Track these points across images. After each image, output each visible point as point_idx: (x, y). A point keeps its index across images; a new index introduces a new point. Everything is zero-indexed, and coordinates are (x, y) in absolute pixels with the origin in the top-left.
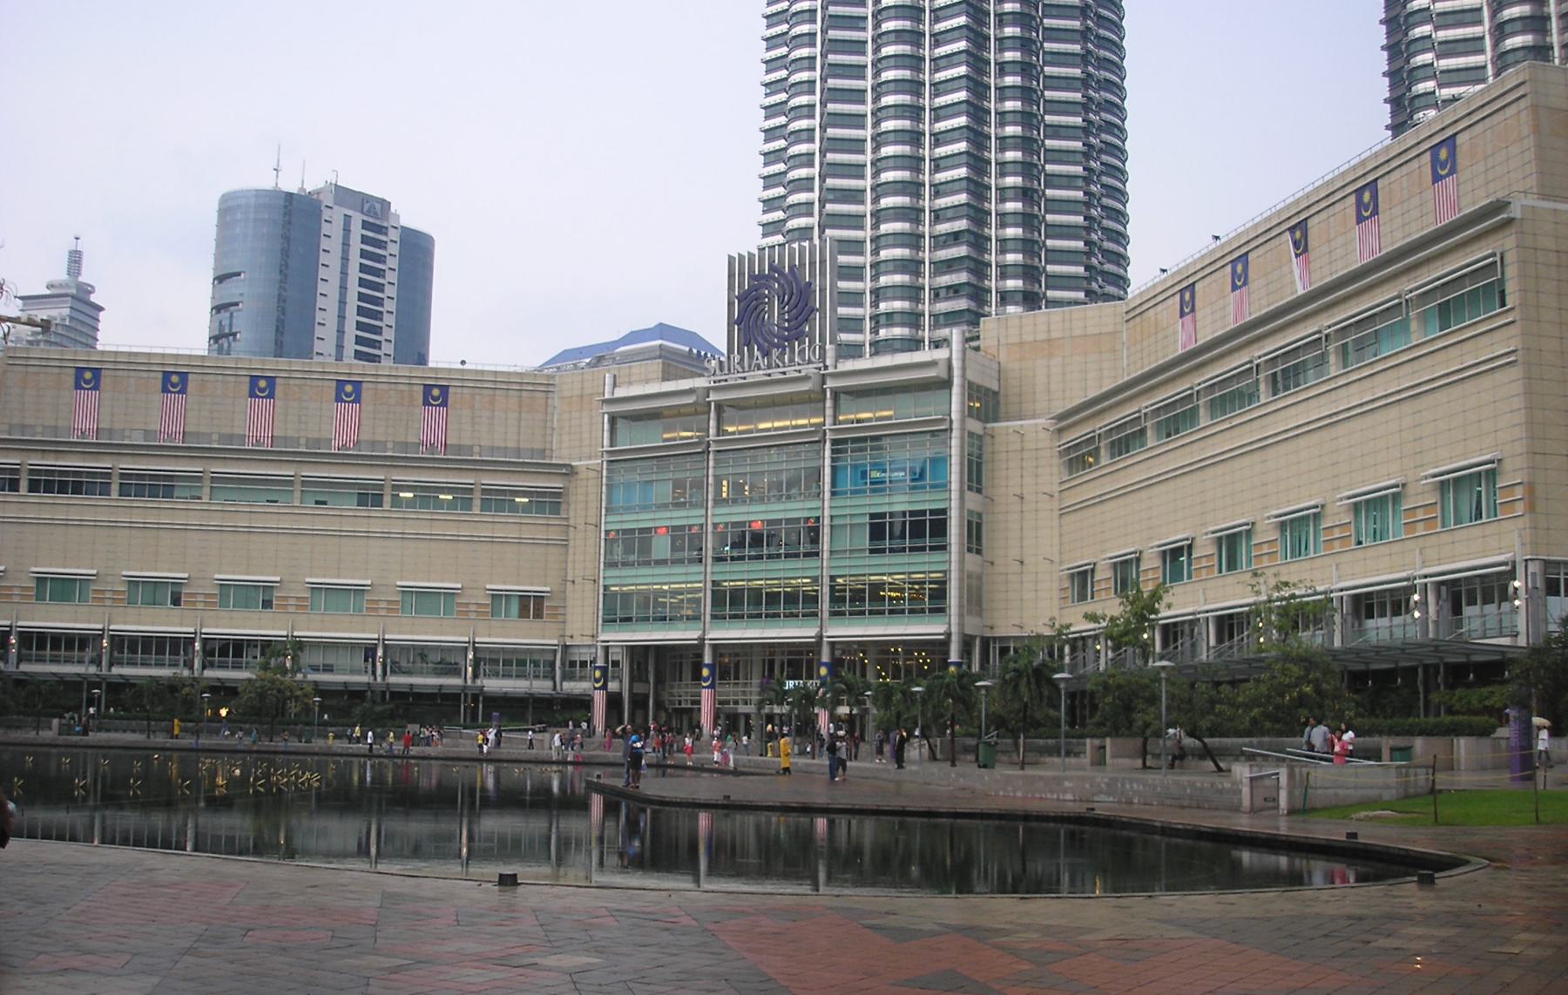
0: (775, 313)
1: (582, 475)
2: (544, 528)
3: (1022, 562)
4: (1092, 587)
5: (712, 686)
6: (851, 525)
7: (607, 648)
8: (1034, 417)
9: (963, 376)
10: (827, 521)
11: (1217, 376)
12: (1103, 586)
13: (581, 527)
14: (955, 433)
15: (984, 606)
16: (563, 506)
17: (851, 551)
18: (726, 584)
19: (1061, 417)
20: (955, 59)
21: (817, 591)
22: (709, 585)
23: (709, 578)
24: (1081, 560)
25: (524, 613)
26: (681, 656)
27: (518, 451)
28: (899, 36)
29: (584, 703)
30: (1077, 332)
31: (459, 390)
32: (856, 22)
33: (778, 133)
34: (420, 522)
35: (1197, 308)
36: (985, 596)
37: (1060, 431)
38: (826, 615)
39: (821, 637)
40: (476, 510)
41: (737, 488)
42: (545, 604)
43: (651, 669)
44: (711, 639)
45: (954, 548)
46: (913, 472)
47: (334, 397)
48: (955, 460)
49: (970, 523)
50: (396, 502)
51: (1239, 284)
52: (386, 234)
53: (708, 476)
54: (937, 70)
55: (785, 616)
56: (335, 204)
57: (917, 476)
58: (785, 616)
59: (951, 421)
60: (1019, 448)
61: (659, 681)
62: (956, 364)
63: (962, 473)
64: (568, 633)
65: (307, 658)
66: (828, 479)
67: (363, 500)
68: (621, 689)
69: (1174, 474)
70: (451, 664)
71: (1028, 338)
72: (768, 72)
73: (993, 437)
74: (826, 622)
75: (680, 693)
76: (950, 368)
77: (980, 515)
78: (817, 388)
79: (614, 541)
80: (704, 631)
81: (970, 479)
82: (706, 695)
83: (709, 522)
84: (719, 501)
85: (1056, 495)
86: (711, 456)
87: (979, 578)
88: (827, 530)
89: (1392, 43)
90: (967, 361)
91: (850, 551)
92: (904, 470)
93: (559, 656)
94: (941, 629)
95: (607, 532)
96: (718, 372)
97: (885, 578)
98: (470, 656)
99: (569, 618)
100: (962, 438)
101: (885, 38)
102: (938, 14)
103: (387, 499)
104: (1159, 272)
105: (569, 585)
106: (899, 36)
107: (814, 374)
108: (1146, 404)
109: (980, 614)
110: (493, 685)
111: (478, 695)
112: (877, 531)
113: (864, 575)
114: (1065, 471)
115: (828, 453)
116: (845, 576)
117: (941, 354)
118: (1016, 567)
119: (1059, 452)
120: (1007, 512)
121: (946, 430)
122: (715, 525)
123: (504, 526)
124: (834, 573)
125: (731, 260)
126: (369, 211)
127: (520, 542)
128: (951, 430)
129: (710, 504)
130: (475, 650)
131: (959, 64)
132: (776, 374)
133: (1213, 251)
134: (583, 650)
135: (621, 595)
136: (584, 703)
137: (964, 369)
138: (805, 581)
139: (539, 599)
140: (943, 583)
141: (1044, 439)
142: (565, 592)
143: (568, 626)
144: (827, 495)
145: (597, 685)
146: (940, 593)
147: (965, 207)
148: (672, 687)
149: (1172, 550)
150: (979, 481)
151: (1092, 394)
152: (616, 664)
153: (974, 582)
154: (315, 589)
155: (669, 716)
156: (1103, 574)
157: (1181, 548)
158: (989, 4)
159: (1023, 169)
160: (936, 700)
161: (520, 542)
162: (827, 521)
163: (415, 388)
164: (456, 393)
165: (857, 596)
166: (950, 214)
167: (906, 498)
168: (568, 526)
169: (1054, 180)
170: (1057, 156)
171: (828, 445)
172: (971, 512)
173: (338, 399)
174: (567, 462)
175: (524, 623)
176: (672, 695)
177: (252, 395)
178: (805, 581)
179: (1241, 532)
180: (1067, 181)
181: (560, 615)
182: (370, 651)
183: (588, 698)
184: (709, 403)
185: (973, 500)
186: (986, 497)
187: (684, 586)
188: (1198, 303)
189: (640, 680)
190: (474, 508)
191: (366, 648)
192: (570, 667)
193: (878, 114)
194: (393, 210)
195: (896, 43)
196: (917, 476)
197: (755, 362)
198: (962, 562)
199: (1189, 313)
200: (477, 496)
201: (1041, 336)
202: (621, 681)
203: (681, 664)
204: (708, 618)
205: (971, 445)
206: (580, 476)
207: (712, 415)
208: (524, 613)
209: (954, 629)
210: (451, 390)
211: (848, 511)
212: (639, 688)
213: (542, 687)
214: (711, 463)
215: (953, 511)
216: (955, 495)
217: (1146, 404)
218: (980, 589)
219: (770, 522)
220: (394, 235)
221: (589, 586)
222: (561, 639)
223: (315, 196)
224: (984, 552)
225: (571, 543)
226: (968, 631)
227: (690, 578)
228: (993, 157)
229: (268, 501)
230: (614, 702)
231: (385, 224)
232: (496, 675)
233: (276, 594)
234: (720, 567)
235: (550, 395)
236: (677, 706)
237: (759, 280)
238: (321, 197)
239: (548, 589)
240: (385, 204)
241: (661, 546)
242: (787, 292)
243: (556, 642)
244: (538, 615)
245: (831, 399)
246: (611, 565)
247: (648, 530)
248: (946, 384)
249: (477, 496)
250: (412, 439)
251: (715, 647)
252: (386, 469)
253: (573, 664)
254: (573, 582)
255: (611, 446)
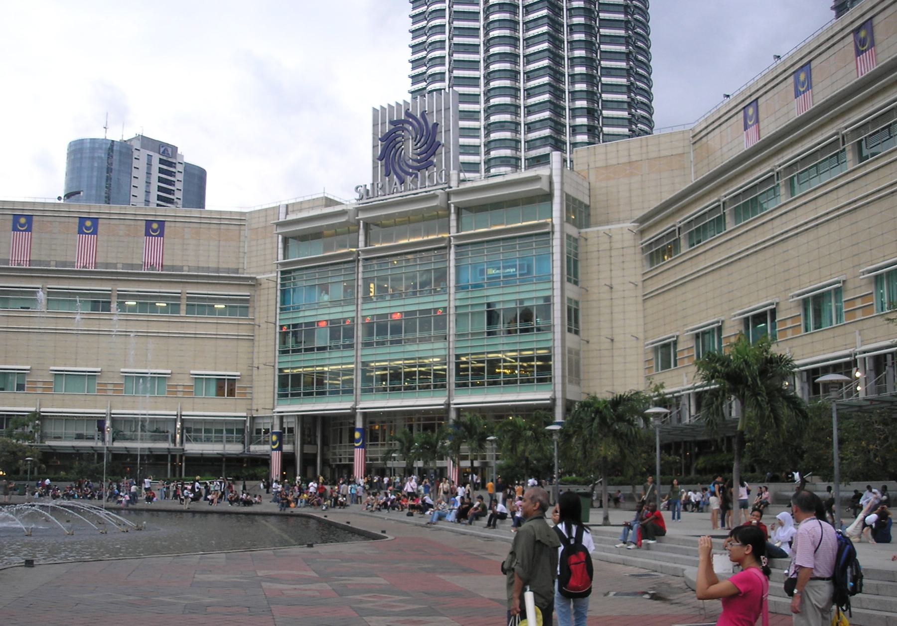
0: (410, 149)
1: (264, 286)
2: (235, 327)
3: (612, 340)
4: (675, 356)
5: (363, 446)
6: (472, 313)
7: (281, 418)
8: (619, 221)
9: (562, 190)
10: (452, 311)
11: (799, 155)
12: (686, 354)
13: (263, 326)
14: (557, 235)
15: (582, 377)
16: (251, 310)
17: (473, 334)
18: (373, 364)
19: (642, 220)
20: (540, 22)
21: (445, 370)
22: (360, 366)
23: (359, 360)
24: (664, 334)
25: (220, 392)
26: (341, 424)
27: (218, 270)
28: (502, 23)
29: (265, 461)
30: (652, 155)
31: (173, 224)
32: (474, 16)
33: (421, 78)
34: (140, 324)
35: (761, 119)
36: (582, 368)
37: (642, 232)
38: (453, 386)
39: (449, 405)
40: (183, 313)
41: (381, 289)
42: (237, 385)
43: (319, 435)
44: (361, 409)
45: (558, 329)
46: (521, 267)
47: (77, 230)
48: (557, 257)
49: (569, 310)
50: (121, 305)
51: (802, 90)
52: (175, 167)
53: (358, 279)
54: (528, 47)
55: (419, 389)
56: (142, 148)
57: (525, 271)
58: (419, 389)
59: (553, 226)
60: (609, 248)
61: (325, 443)
62: (556, 180)
63: (562, 267)
64: (255, 407)
65: (50, 429)
66: (452, 277)
67: (95, 305)
68: (294, 450)
69: (755, 250)
70: (164, 432)
71: (613, 162)
72: (413, 38)
73: (586, 239)
74: (453, 392)
75: (339, 453)
76: (551, 183)
77: (577, 303)
78: (444, 205)
79: (286, 333)
80: (356, 402)
81: (569, 273)
82: (358, 454)
83: (359, 316)
84: (367, 299)
85: (640, 284)
86: (361, 264)
87: (577, 353)
88: (453, 318)
89: (838, 4)
90: (565, 177)
91: (472, 334)
92: (515, 266)
93: (248, 424)
94: (548, 395)
95: (281, 327)
96: (365, 197)
97: (500, 355)
98: (178, 426)
99: (255, 395)
100: (562, 239)
101: (492, 59)
102: (528, 9)
103: (114, 305)
104: (722, 98)
105: (255, 372)
106: (502, 23)
107: (441, 193)
108: (724, 194)
109: (578, 384)
110: (193, 448)
111: (183, 455)
112: (492, 317)
113: (483, 353)
114: (647, 263)
115: (452, 256)
116: (467, 354)
117: (542, 171)
118: (607, 344)
119: (642, 249)
120: (599, 300)
121: (548, 233)
122: (364, 317)
123: (204, 326)
124: (459, 352)
125: (374, 110)
126: (164, 152)
127: (216, 338)
128: (553, 233)
129: (360, 301)
130: (183, 421)
131: (543, 25)
132: (410, 194)
133: (776, 68)
134: (266, 421)
135: (292, 375)
136: (265, 461)
137: (562, 184)
138: (435, 360)
139: (232, 382)
140: (546, 359)
141: (629, 236)
142: (252, 375)
143: (255, 401)
144: (452, 290)
145: (274, 447)
146: (545, 369)
147: (549, 121)
148: (334, 448)
149: (754, 317)
150: (576, 275)
151: (667, 196)
152: (291, 430)
153: (574, 357)
154: (58, 375)
155: (333, 473)
156: (686, 344)
157: (765, 313)
158: (563, 2)
159: (587, 95)
160: (586, 432)
161: (216, 338)
162: (452, 311)
163: (139, 223)
164: (170, 227)
165: (478, 372)
166: (538, 125)
167: (505, 340)
168: (254, 325)
169: (607, 104)
170: (609, 88)
171: (453, 250)
172: (569, 300)
173: (80, 232)
174: (253, 276)
175: (220, 401)
176: (334, 454)
177: (15, 229)
178: (435, 360)
179: (829, 292)
180: (617, 105)
181: (248, 394)
182: (101, 423)
183: (267, 457)
184: (358, 221)
185: (572, 291)
186: (581, 288)
187: (340, 367)
188: (762, 115)
189: (310, 443)
190: (181, 312)
191: (98, 421)
192: (257, 433)
193: (489, 111)
194: (179, 152)
195: (499, 12)
196: (525, 271)
197: (394, 186)
198: (563, 340)
199: (753, 125)
200: (184, 302)
201: (624, 160)
202: (294, 444)
203: (341, 429)
204: (359, 392)
205: (569, 245)
206: (262, 287)
207: (362, 232)
208: (220, 392)
209: (559, 395)
210: (166, 224)
211: (469, 302)
212: (309, 449)
213: (234, 449)
214: (361, 269)
215: (555, 299)
216: (557, 285)
217: (724, 194)
218: (578, 363)
219: (407, 313)
220: (180, 168)
221: (270, 371)
222: (249, 412)
223: (129, 143)
224: (581, 333)
225: (257, 338)
226: (570, 397)
227: (345, 361)
228: (566, 87)
229: (22, 308)
230: (288, 461)
231: (174, 161)
232: (196, 440)
233: (27, 379)
234: (368, 351)
235: (242, 228)
236: (338, 463)
237: (397, 125)
238: (132, 143)
239: (238, 373)
240: (175, 149)
241: (322, 338)
242: (419, 132)
243: (245, 414)
244: (231, 393)
245: (455, 213)
246: (284, 352)
247: (312, 324)
248: (548, 197)
249: (184, 302)
250: (137, 261)
251: (365, 415)
252: (112, 283)
253: (258, 431)
254: (258, 368)
255: (284, 259)
